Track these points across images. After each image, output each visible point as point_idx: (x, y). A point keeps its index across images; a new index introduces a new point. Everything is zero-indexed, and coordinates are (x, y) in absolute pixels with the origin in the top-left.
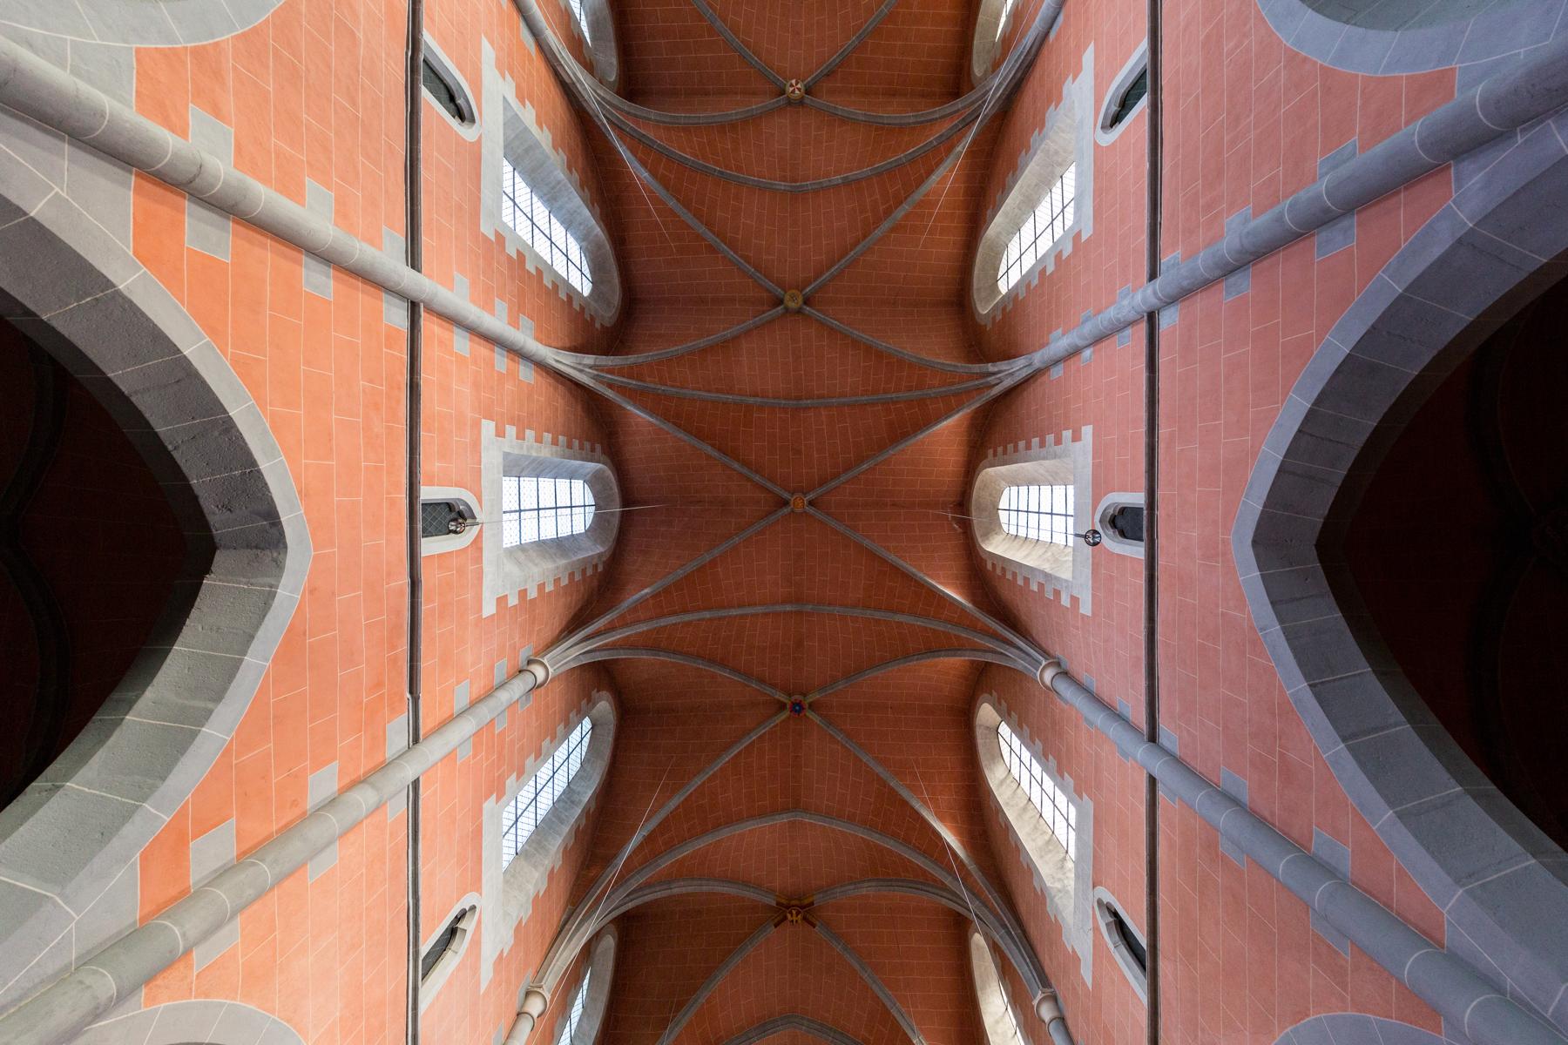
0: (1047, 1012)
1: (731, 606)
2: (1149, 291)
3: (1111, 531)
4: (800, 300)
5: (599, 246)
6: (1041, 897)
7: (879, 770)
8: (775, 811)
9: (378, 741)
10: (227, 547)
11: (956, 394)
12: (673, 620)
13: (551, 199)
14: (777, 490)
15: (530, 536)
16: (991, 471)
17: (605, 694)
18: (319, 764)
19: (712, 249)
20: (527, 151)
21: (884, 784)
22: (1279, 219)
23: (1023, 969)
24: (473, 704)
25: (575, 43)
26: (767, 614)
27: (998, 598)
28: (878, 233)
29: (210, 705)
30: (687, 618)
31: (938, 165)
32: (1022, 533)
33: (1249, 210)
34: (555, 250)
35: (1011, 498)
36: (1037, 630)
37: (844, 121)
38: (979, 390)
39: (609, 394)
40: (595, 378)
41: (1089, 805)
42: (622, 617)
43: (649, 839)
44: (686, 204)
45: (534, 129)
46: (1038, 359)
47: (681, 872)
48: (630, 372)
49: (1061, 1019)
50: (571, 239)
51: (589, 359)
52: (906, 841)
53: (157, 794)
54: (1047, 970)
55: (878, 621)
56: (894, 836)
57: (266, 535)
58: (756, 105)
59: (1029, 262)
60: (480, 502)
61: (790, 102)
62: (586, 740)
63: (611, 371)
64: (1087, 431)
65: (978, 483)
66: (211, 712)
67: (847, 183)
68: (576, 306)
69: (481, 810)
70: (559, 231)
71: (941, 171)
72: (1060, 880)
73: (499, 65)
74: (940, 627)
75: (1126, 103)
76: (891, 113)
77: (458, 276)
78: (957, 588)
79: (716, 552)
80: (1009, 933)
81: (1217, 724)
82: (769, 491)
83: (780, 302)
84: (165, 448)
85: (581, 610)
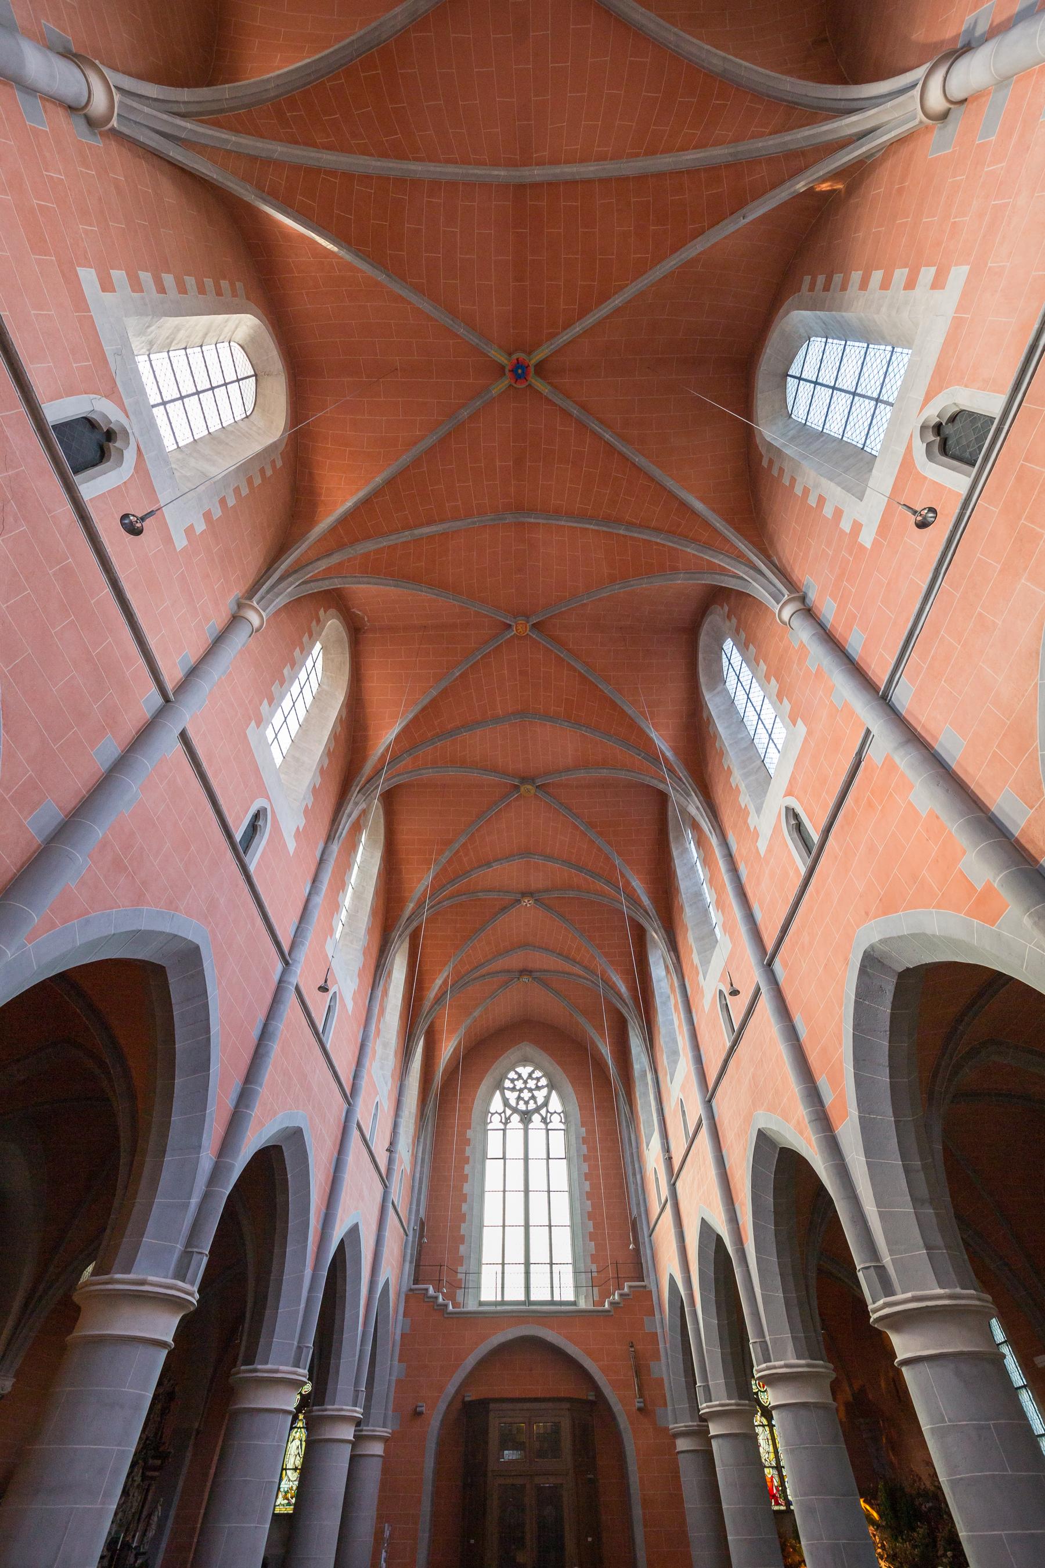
10: (894, 971)
15: (879, 353)
19: (592, 825)
28: (462, 840)
34: (747, 688)
35: (235, 404)
45: (743, 787)
50: (732, 692)
52: (348, 177)
56: (366, 178)
57: (872, 963)
60: (909, 449)
70: (740, 700)
75: (253, 828)
78: (287, 235)
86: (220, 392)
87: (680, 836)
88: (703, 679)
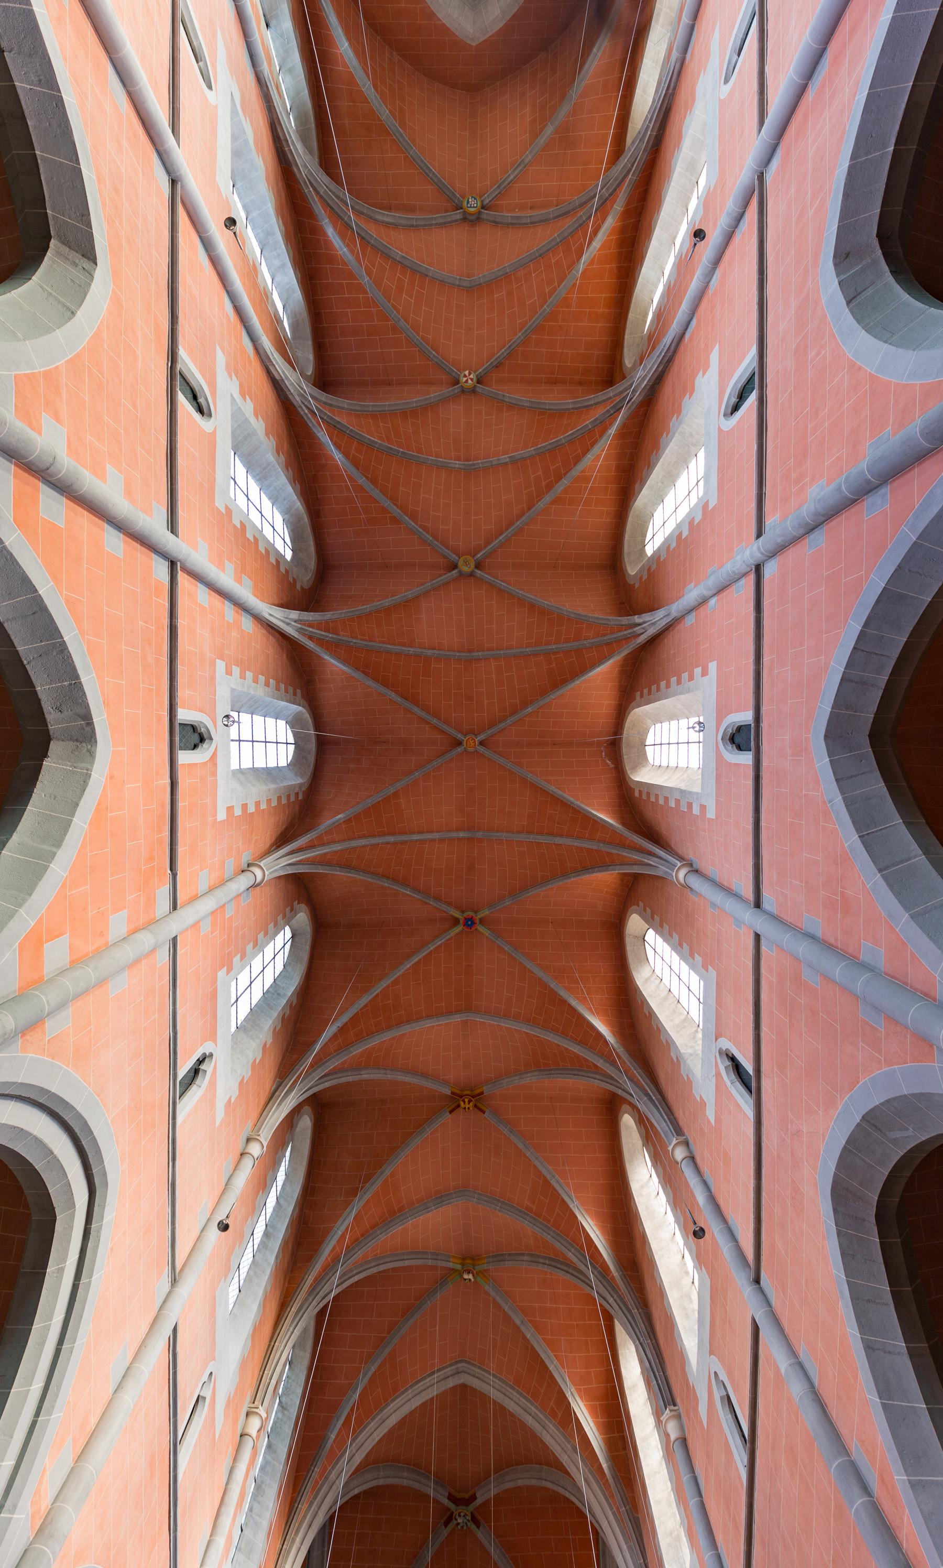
0: (679, 1154)
1: (412, 833)
2: (755, 548)
3: (730, 746)
4: (473, 565)
5: (299, 518)
6: (677, 1064)
7: (541, 974)
8: (450, 1012)
9: (151, 902)
11: (608, 644)
12: (362, 842)
13: (262, 478)
14: (453, 732)
16: (637, 710)
17: (303, 906)
18: (117, 909)
19: (396, 521)
20: (246, 438)
21: (544, 986)
22: (839, 489)
23: (660, 1123)
24: (211, 889)
25: (281, 345)
26: (442, 840)
27: (643, 819)
28: (541, 505)
29: (54, 849)
30: (374, 841)
31: (593, 444)
32: (664, 764)
33: (823, 482)
35: (657, 734)
36: (675, 840)
37: (511, 407)
38: (627, 639)
39: (310, 644)
40: (299, 630)
41: (712, 973)
42: (320, 837)
43: (343, 1030)
44: (374, 481)
45: (252, 420)
46: (675, 609)
47: (369, 1061)
48: (326, 626)
49: (692, 1158)
51: (294, 614)
52: (564, 1034)
53: (27, 904)
54: (681, 1123)
55: (539, 844)
56: (554, 1030)
58: (435, 394)
59: (670, 527)
61: (463, 391)
62: (288, 947)
63: (311, 625)
64: (713, 666)
65: (628, 723)
66: (54, 854)
67: (514, 461)
68: (283, 570)
69: (216, 977)
70: (267, 505)
71: (596, 450)
72: (692, 1047)
73: (228, 369)
74: (593, 846)
75: (742, 396)
76: (555, 399)
77: (200, 542)
79: (399, 785)
80: (651, 1099)
81: (801, 882)
82: (442, 732)
83: (455, 566)
84: (22, 662)
85: (286, 829)
86: (665, 741)
87: (295, 327)
88: (306, 519)
